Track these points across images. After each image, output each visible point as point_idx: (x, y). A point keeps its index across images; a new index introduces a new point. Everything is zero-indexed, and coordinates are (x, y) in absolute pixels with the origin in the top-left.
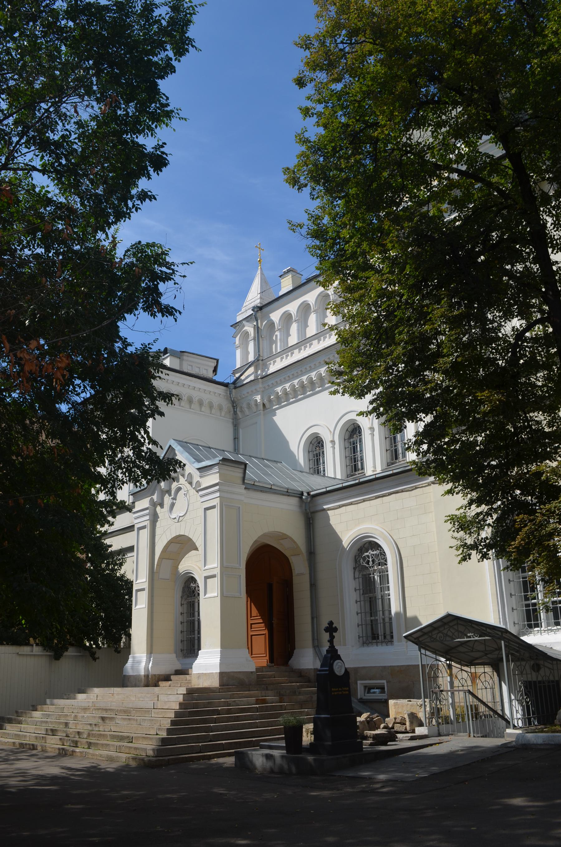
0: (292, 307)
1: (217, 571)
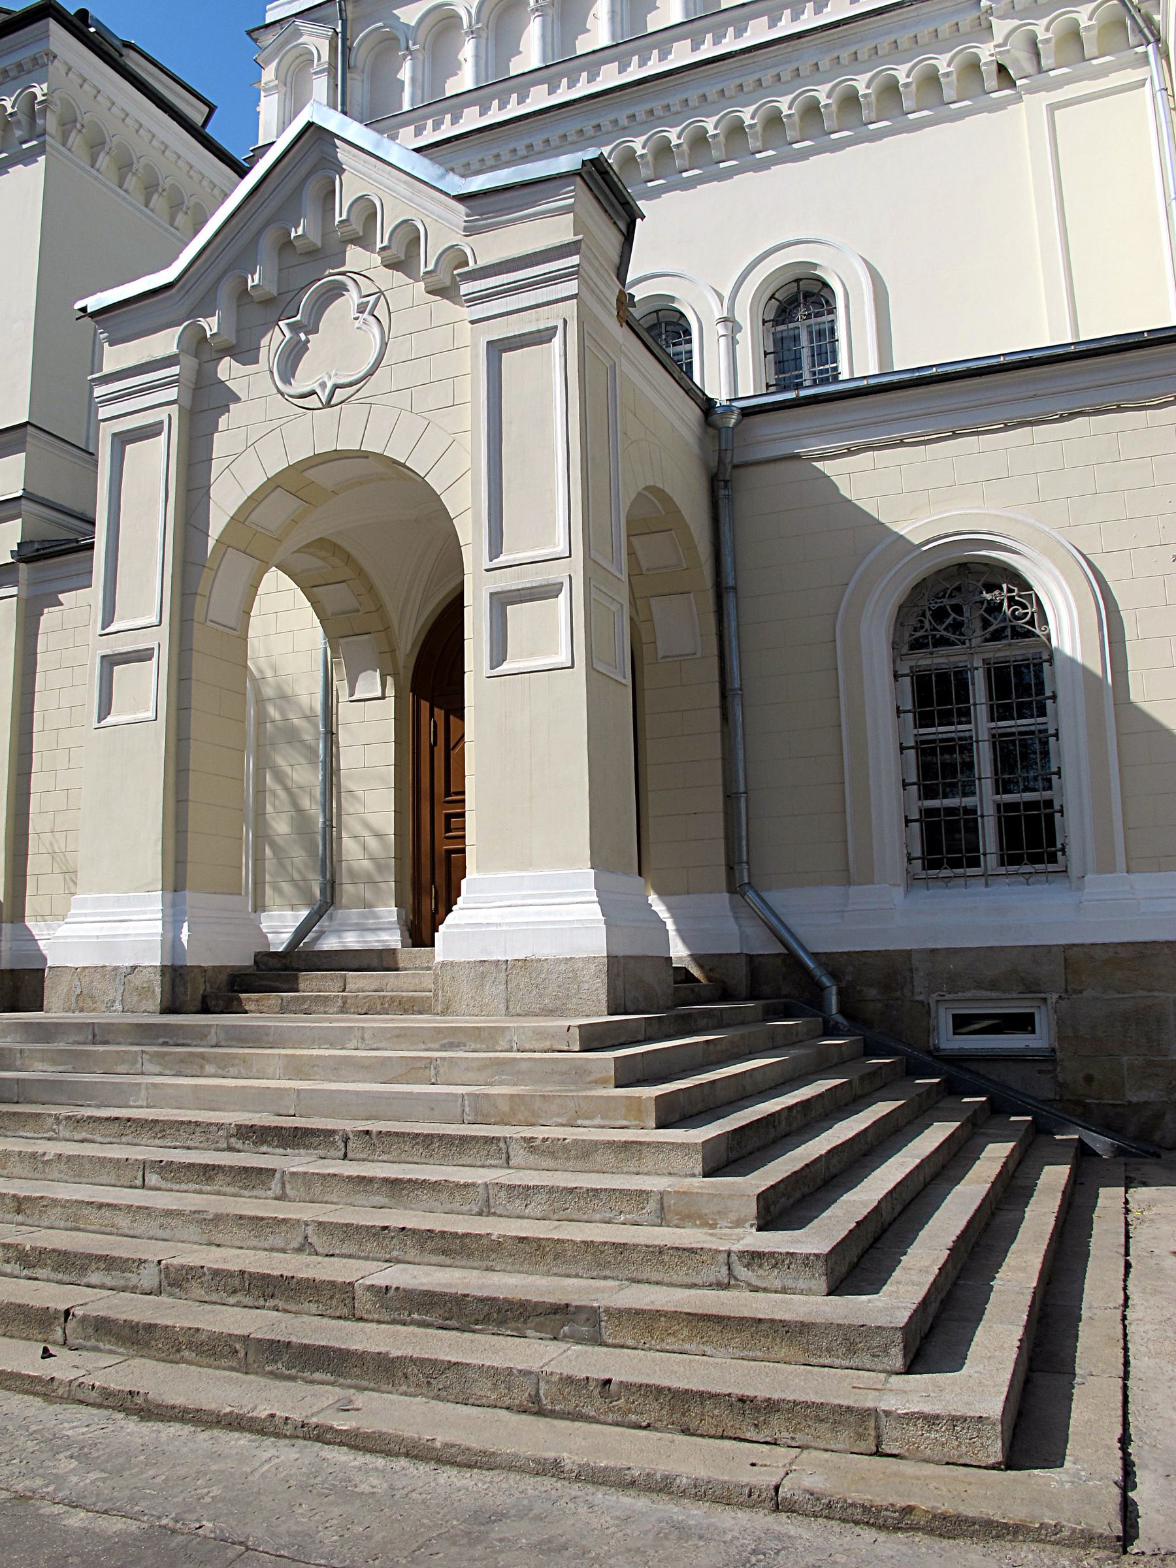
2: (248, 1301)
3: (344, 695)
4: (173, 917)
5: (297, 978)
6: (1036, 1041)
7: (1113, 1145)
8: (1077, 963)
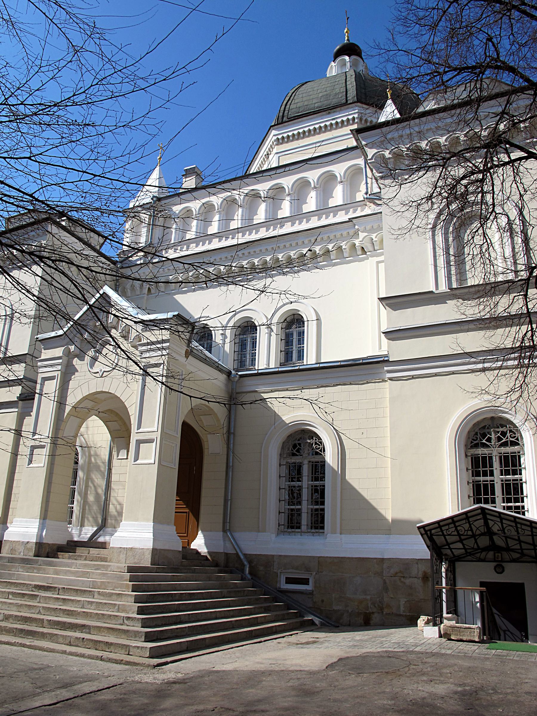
0: (195, 205)
1: (157, 436)
2: (21, 623)
3: (115, 457)
4: (42, 527)
5: (76, 549)
6: (308, 588)
7: (321, 622)
8: (323, 563)
